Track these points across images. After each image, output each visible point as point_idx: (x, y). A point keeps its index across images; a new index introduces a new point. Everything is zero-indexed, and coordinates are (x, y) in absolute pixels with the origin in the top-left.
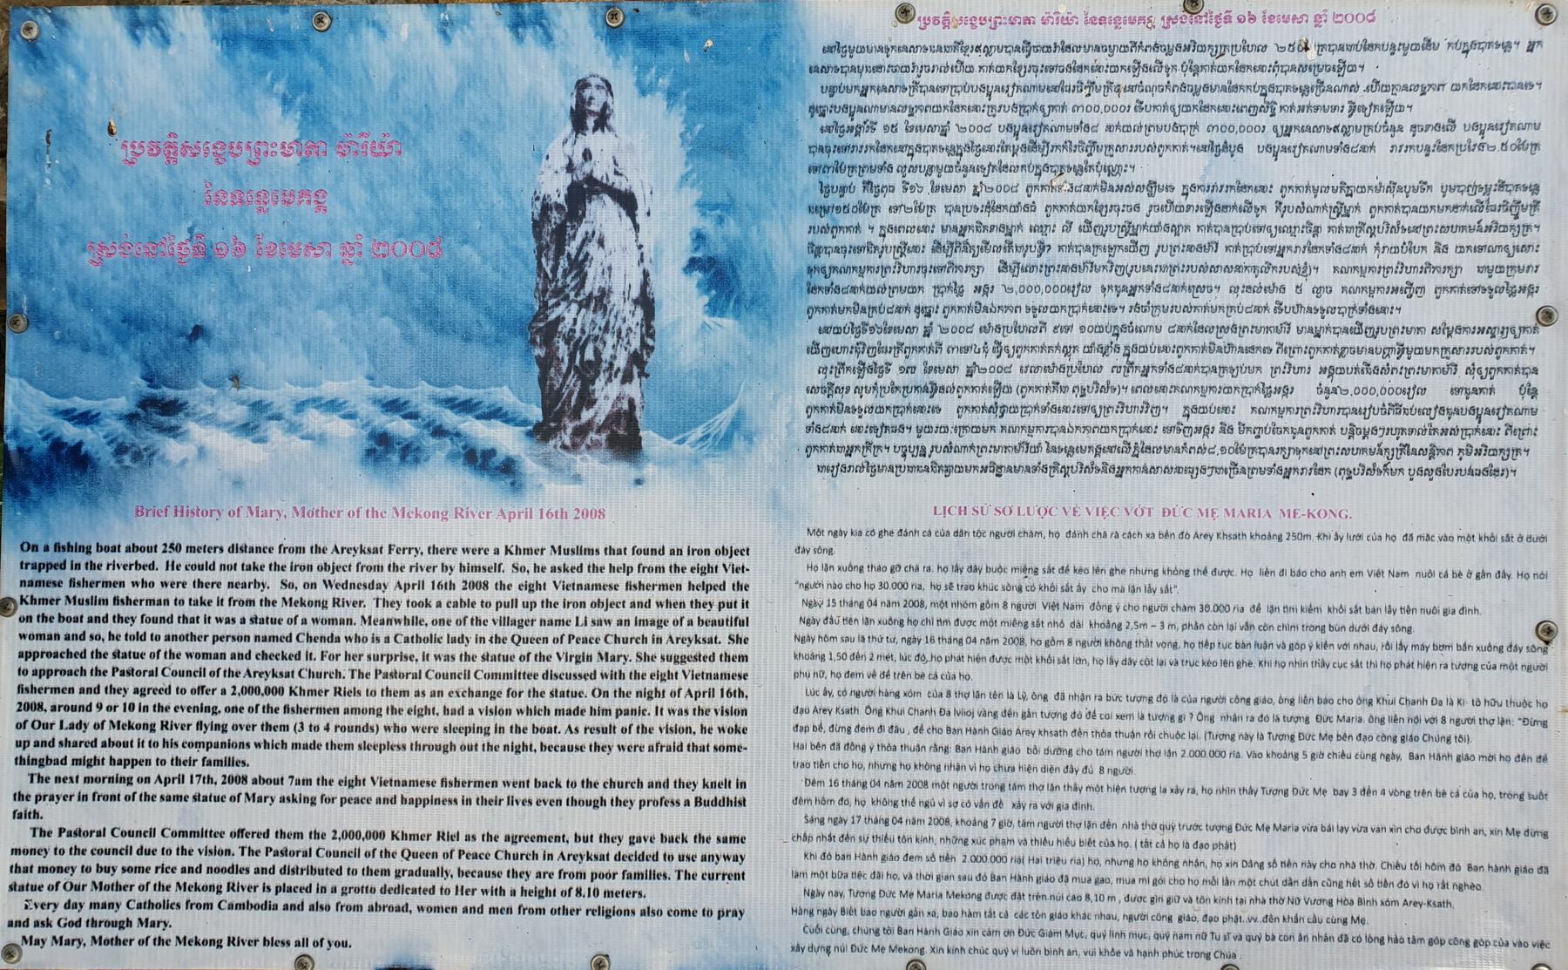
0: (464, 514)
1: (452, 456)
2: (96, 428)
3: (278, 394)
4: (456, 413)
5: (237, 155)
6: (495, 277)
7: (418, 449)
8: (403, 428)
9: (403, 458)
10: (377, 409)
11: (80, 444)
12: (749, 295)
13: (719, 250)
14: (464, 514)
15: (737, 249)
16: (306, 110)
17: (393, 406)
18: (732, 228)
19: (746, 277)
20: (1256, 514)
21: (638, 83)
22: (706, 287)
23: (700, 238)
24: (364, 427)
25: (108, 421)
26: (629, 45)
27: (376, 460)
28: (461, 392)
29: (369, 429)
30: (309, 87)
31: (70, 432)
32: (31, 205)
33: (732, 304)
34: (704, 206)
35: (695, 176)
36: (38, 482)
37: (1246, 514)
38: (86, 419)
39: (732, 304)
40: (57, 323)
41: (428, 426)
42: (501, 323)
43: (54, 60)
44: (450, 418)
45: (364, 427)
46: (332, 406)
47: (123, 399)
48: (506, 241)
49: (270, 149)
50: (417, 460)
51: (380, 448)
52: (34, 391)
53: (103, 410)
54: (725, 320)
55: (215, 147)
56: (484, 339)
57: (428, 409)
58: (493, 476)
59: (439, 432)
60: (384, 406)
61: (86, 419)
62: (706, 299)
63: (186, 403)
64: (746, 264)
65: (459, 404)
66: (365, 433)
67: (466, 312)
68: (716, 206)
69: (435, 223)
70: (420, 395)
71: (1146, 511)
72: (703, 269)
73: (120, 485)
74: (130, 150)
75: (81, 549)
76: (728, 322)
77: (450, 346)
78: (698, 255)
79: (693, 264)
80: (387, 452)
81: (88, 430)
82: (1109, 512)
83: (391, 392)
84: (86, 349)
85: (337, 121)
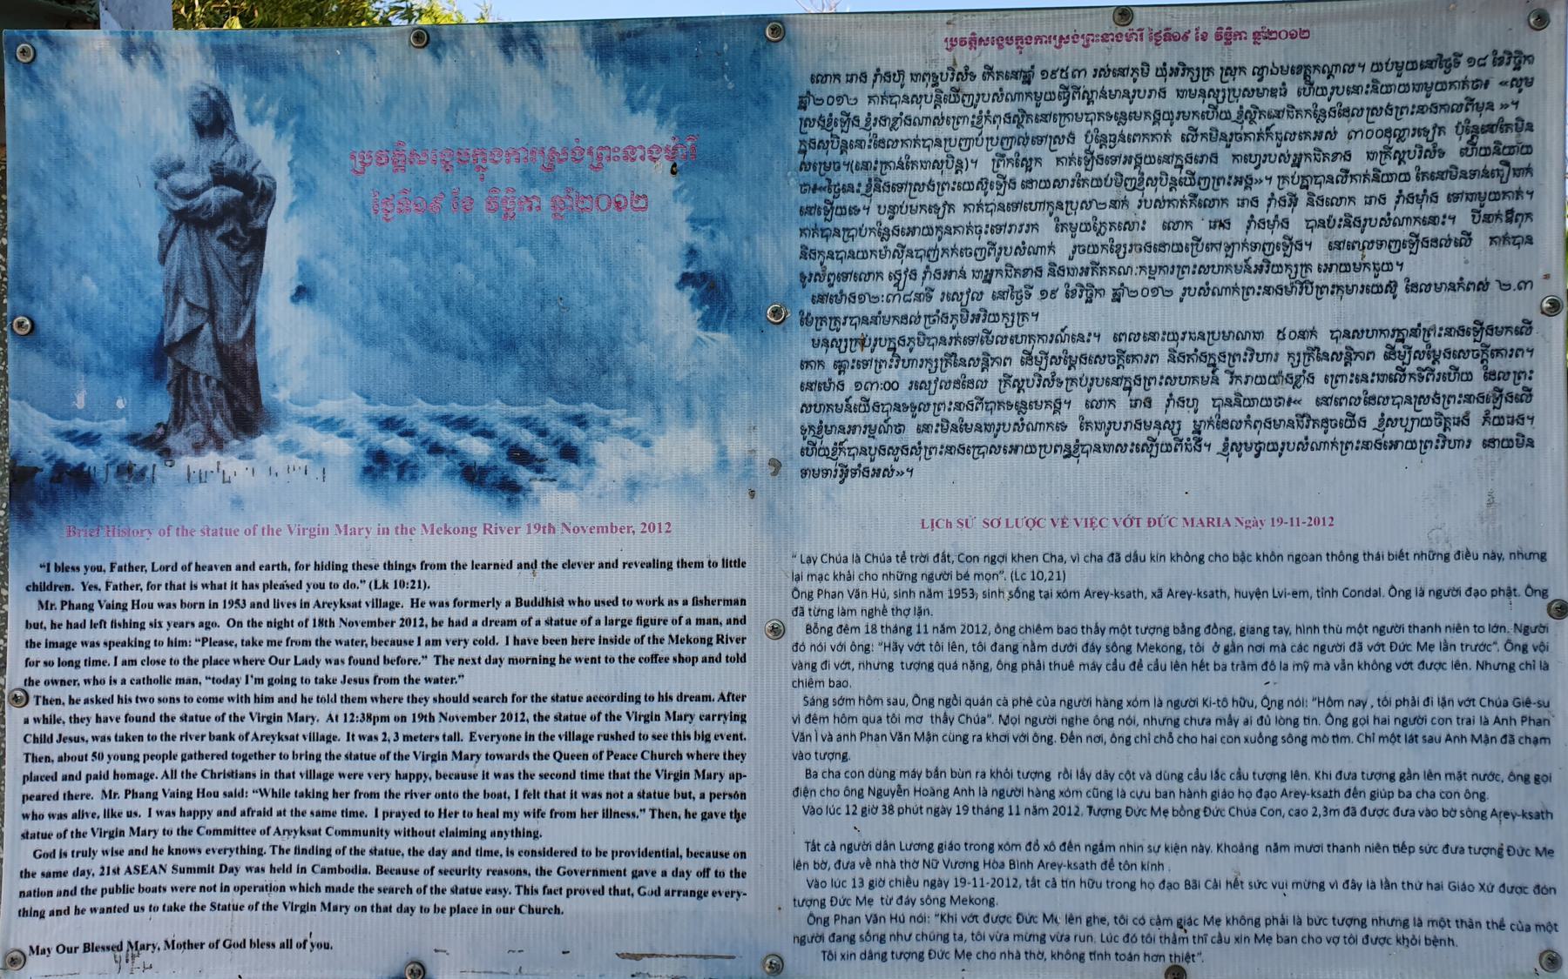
0: (493, 530)
1: (449, 473)
2: (99, 449)
3: (543, 411)
4: (453, 430)
5: (496, 162)
6: (112, 308)
7: (415, 466)
8: (399, 445)
9: (400, 475)
10: (372, 427)
11: (83, 465)
12: (742, 309)
13: (710, 264)
14: (493, 530)
15: (727, 261)
16: (299, 132)
17: (389, 424)
18: (724, 243)
19: (739, 292)
20: (1215, 523)
21: (629, 101)
22: (697, 302)
23: (692, 253)
24: (556, 443)
25: (108, 442)
26: (618, 63)
27: (375, 477)
28: (457, 409)
29: (366, 447)
30: (301, 110)
31: (73, 454)
32: (31, 230)
33: (725, 317)
34: (695, 222)
35: (686, 191)
36: (42, 503)
37: (1205, 522)
38: (88, 440)
39: (725, 317)
40: (57, 345)
41: (424, 443)
42: (118, 355)
43: (51, 85)
44: (445, 435)
45: (362, 444)
46: (329, 424)
47: (124, 421)
48: (122, 272)
49: (613, 154)
50: (414, 478)
51: (377, 465)
52: (36, 413)
53: (104, 431)
54: (721, 335)
55: (492, 154)
56: (479, 357)
57: (424, 427)
58: (489, 492)
59: (436, 449)
60: (381, 423)
61: (88, 440)
62: (699, 314)
63: (404, 420)
64: (738, 278)
65: (453, 423)
66: (362, 451)
67: (461, 330)
68: (706, 222)
69: (428, 241)
70: (417, 412)
71: (1135, 522)
72: (696, 284)
73: (121, 504)
74: (358, 160)
75: (338, 567)
76: (722, 337)
77: (446, 363)
78: (690, 270)
79: (686, 280)
80: (384, 469)
81: (90, 451)
82: (1097, 523)
83: (386, 410)
84: (462, 356)
85: (329, 142)
